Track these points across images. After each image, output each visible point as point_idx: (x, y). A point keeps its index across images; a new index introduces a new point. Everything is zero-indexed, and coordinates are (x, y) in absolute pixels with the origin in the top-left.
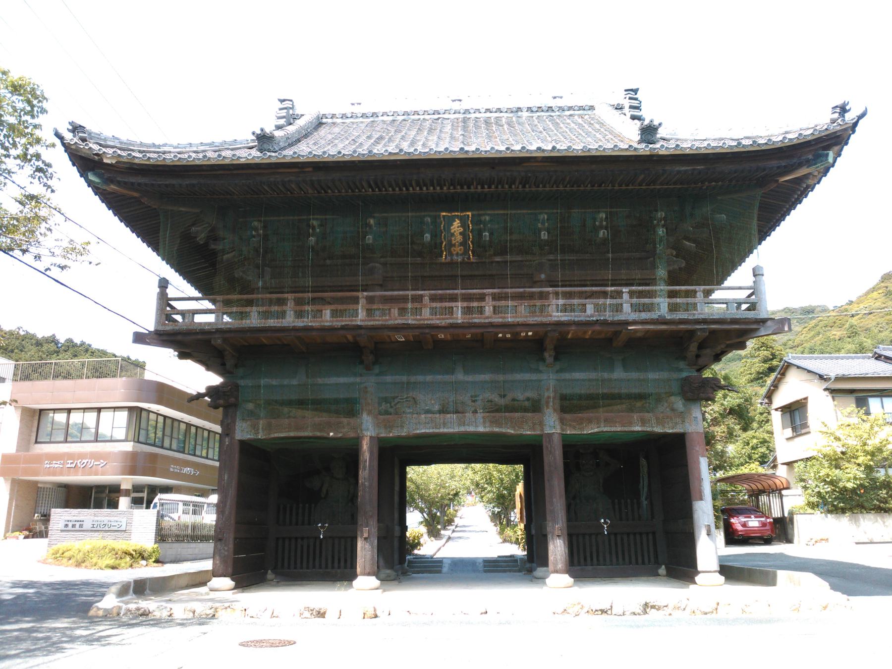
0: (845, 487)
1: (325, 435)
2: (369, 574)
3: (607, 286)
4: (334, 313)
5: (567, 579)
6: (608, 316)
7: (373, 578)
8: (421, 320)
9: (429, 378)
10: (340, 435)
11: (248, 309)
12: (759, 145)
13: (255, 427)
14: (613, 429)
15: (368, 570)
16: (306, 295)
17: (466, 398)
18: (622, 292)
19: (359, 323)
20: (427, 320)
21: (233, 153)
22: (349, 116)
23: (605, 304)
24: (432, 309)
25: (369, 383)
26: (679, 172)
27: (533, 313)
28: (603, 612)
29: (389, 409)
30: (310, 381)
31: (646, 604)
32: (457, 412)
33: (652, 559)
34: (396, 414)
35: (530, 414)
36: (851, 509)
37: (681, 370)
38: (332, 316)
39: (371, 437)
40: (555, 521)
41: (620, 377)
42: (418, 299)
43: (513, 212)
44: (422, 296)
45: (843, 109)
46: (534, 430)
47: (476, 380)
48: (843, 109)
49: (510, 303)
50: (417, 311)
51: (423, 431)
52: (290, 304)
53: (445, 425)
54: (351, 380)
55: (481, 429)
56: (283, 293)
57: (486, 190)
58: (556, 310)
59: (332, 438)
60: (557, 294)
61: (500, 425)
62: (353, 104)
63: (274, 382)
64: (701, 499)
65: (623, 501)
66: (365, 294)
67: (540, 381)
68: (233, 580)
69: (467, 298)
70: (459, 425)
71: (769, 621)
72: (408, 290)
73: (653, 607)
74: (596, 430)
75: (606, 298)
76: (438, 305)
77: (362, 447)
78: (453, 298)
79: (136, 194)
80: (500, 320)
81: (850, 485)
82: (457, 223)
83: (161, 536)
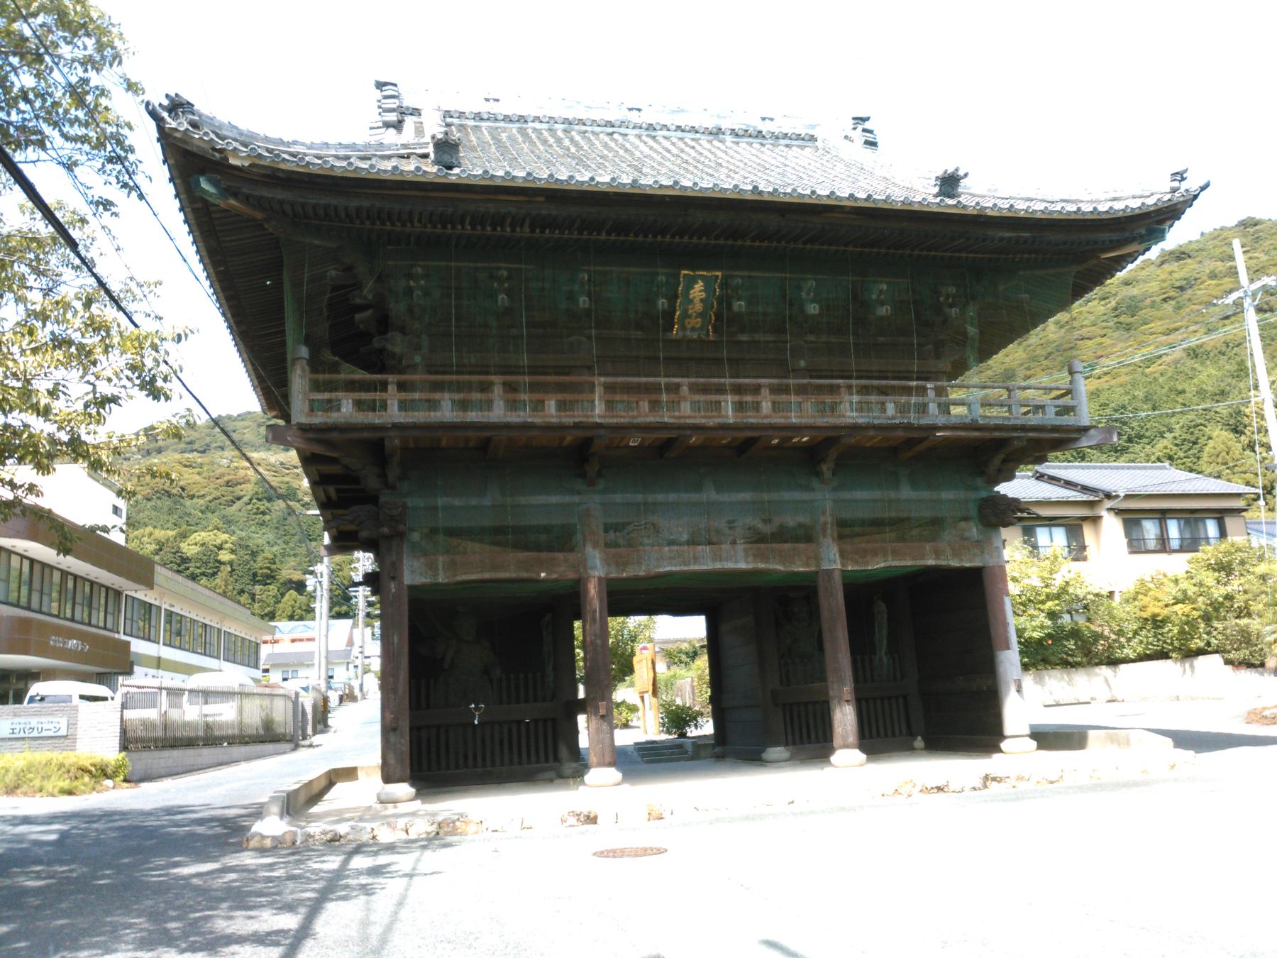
0: (1031, 638)
1: (534, 576)
2: (610, 764)
3: (911, 379)
4: (562, 406)
5: (858, 756)
6: (913, 418)
7: (613, 770)
8: (679, 417)
9: (672, 497)
10: (555, 576)
11: (437, 396)
12: (1100, 213)
13: (432, 567)
14: (903, 563)
15: (608, 759)
16: (520, 378)
17: (721, 523)
18: (925, 389)
19: (598, 420)
20: (689, 417)
21: (1028, 204)
22: (486, 116)
23: (909, 404)
24: (693, 403)
25: (591, 504)
26: (1002, 239)
27: (822, 412)
28: (939, 789)
29: (619, 536)
30: (509, 500)
31: (986, 778)
32: (710, 543)
33: (904, 730)
34: (630, 545)
35: (802, 546)
36: (1035, 665)
37: (977, 489)
38: (400, 409)
39: (600, 579)
40: (841, 681)
41: (909, 496)
42: (675, 389)
43: (598, 268)
44: (678, 386)
45: (1180, 176)
46: (808, 566)
47: (736, 502)
48: (1180, 176)
49: (793, 398)
50: (673, 405)
51: (668, 569)
52: (498, 391)
53: (696, 560)
54: (567, 499)
55: (742, 565)
56: (487, 373)
57: (449, 231)
58: (852, 409)
59: (544, 581)
60: (849, 387)
61: (766, 560)
62: (487, 100)
63: (457, 502)
64: (1008, 648)
65: (530, 675)
66: (603, 379)
67: (813, 501)
68: (412, 785)
69: (738, 390)
70: (714, 560)
71: (1146, 783)
72: (659, 376)
73: (994, 779)
74: (883, 565)
75: (910, 394)
76: (702, 398)
77: (587, 591)
78: (721, 390)
79: (259, 215)
80: (782, 421)
81: (1036, 635)
82: (699, 286)
83: (128, 741)
